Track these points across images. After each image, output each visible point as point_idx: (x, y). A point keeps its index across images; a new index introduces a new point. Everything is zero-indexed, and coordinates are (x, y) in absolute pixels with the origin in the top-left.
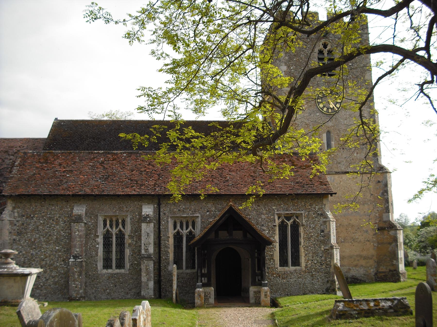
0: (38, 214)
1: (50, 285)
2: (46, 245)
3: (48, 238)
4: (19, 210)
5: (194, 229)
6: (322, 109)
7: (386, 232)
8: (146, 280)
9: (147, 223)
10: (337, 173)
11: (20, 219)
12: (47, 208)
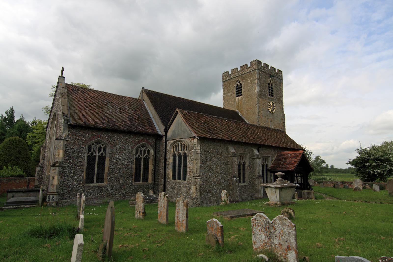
4: (203, 147)
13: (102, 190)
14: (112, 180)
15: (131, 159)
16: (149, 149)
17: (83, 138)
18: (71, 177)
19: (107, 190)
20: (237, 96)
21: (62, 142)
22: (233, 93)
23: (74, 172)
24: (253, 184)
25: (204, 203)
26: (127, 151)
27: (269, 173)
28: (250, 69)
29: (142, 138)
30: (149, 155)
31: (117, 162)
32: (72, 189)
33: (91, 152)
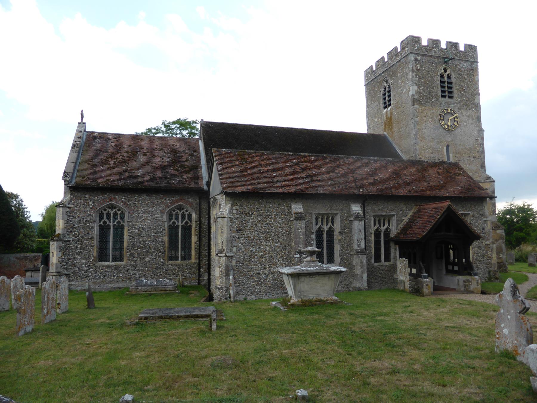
0: (256, 211)
1: (269, 281)
2: (265, 241)
3: (266, 235)
5: (333, 224)
8: (360, 273)
9: (360, 220)
11: (238, 216)
12: (265, 207)
13: (120, 271)
14: (134, 257)
15: (161, 228)
16: (190, 213)
17: (91, 203)
18: (77, 253)
19: (127, 270)
20: (385, 108)
21: (61, 209)
22: (379, 103)
23: (81, 247)
24: (350, 264)
25: (240, 294)
26: (154, 217)
27: (392, 245)
28: (401, 55)
29: (177, 197)
30: (191, 222)
31: (139, 232)
32: (79, 268)
33: (172, 221)
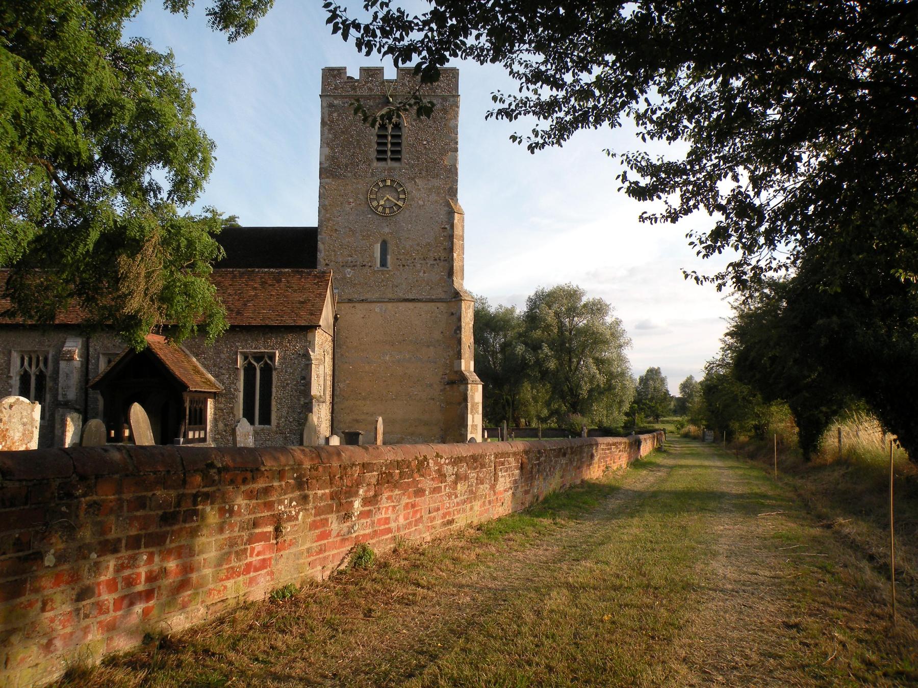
6: (376, 208)
7: (455, 386)
10: (391, 301)
